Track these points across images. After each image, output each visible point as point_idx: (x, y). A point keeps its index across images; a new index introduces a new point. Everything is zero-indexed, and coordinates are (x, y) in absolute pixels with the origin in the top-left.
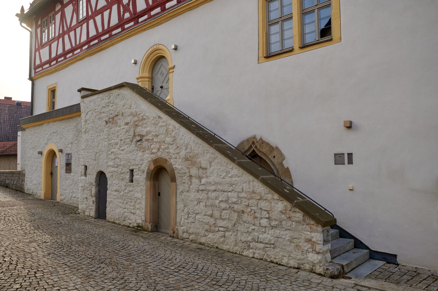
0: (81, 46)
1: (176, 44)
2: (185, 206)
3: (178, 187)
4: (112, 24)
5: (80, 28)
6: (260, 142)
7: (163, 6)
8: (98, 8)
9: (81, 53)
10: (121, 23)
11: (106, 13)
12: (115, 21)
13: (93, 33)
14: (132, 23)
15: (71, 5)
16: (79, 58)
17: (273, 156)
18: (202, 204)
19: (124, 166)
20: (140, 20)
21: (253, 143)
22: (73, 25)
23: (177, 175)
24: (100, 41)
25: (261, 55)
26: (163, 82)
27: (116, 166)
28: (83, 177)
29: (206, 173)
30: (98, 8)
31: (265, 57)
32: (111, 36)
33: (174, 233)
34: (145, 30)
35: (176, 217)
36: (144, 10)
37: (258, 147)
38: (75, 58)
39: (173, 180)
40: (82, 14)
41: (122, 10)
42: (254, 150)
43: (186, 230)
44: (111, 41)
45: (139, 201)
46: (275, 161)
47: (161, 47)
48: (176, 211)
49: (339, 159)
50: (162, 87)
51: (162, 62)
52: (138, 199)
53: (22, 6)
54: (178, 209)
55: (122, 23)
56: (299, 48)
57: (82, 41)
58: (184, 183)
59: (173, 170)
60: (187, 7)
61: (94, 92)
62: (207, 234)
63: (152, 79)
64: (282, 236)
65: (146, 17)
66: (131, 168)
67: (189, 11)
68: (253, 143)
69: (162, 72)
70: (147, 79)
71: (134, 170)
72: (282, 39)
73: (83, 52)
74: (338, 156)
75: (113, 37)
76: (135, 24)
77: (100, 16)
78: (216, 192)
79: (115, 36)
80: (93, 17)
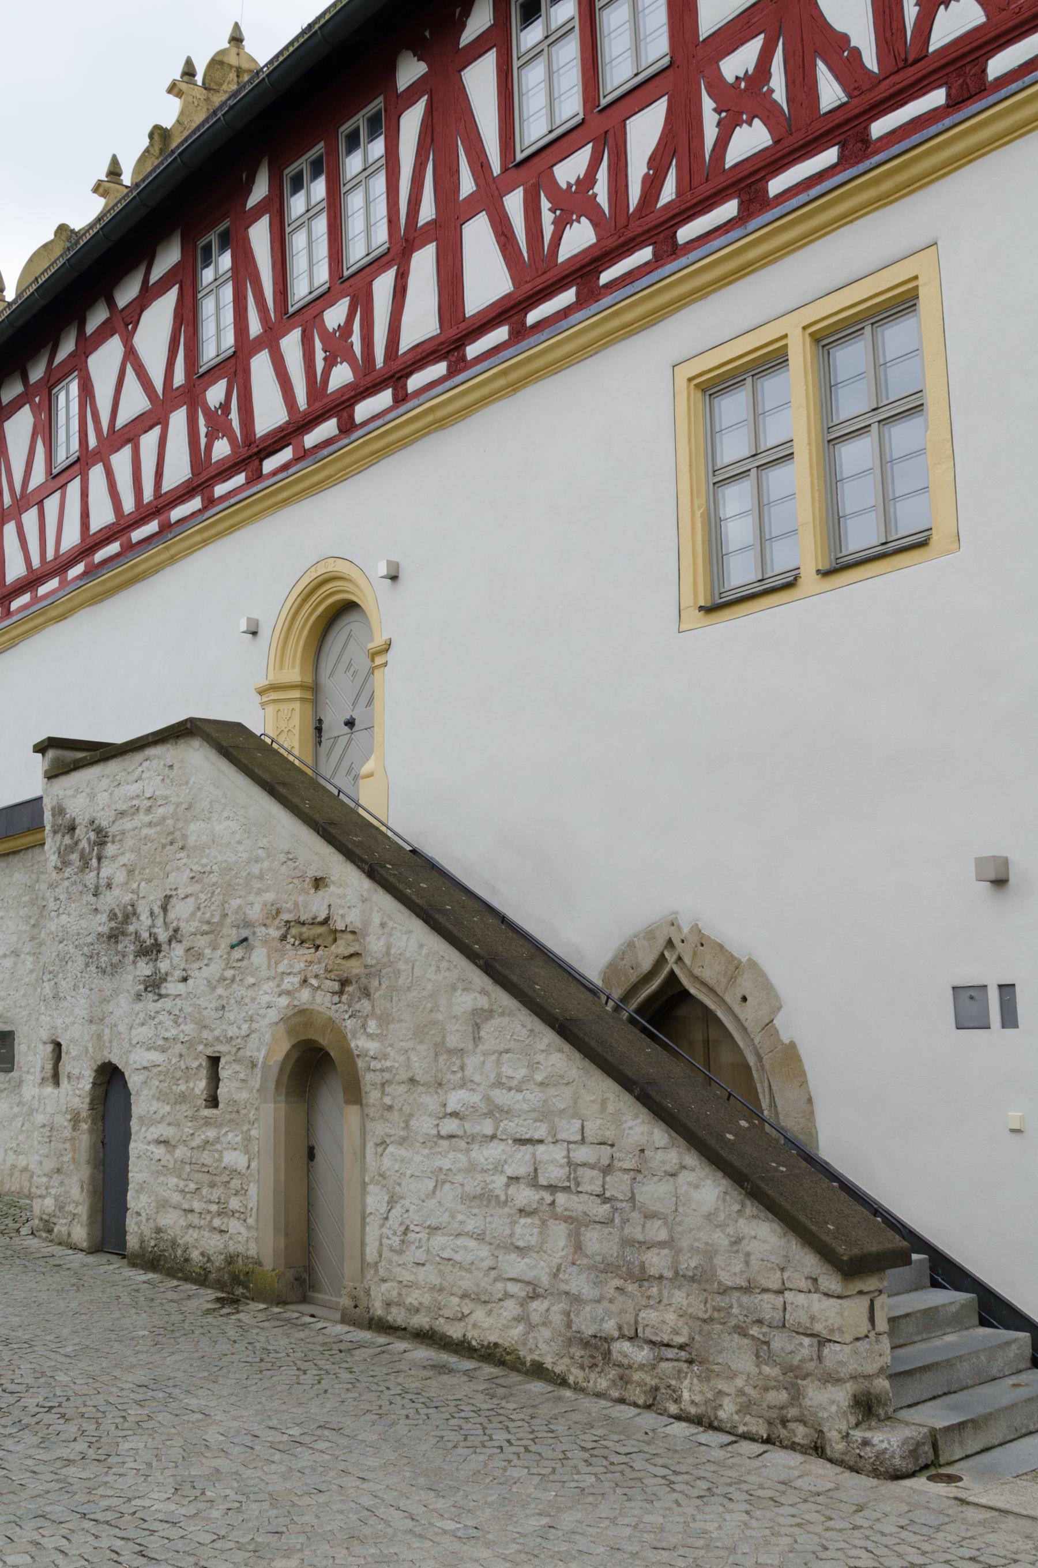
0: (60, 566)
1: (395, 559)
2: (392, 1202)
3: (370, 1125)
4: (169, 484)
5: (57, 495)
6: (693, 940)
7: (345, 414)
8: (121, 421)
9: (62, 593)
10: (202, 480)
11: (149, 441)
12: (178, 470)
13: (102, 516)
14: (240, 479)
15: (27, 408)
16: (53, 613)
17: (740, 996)
18: (447, 1193)
19: (190, 1044)
20: (270, 465)
21: (670, 944)
22: (33, 485)
23: (368, 1078)
24: (129, 548)
25: (688, 600)
26: (354, 704)
27: (160, 1042)
28: (49, 1090)
29: (462, 1068)
30: (120, 423)
31: (701, 608)
32: (166, 527)
33: (356, 1307)
34: (286, 502)
35: (363, 1244)
36: (281, 429)
37: (687, 961)
38: (43, 611)
39: (354, 1094)
40: (67, 448)
41: (203, 430)
42: (672, 973)
43: (395, 1293)
44: (167, 548)
45: (236, 1183)
46: (748, 1014)
47: (341, 567)
48: (363, 1218)
49: (970, 1007)
50: (350, 723)
51: (348, 625)
52: (234, 1172)
53: (236, 24)
54: (369, 1210)
55: (204, 477)
56: (818, 572)
57: (167, 486)
58: (390, 1108)
59: (350, 1057)
60: (430, 418)
61: (99, 753)
62: (466, 1311)
63: (313, 691)
64: (716, 1315)
65: (286, 454)
66: (209, 1052)
67: (436, 430)
68: (670, 944)
69: (350, 665)
70: (297, 694)
71: (223, 1061)
72: (887, 501)
73: (68, 589)
74: (964, 996)
75: (176, 530)
76: (249, 482)
77: (126, 452)
78: (494, 1144)
79: (180, 528)
80: (101, 455)
